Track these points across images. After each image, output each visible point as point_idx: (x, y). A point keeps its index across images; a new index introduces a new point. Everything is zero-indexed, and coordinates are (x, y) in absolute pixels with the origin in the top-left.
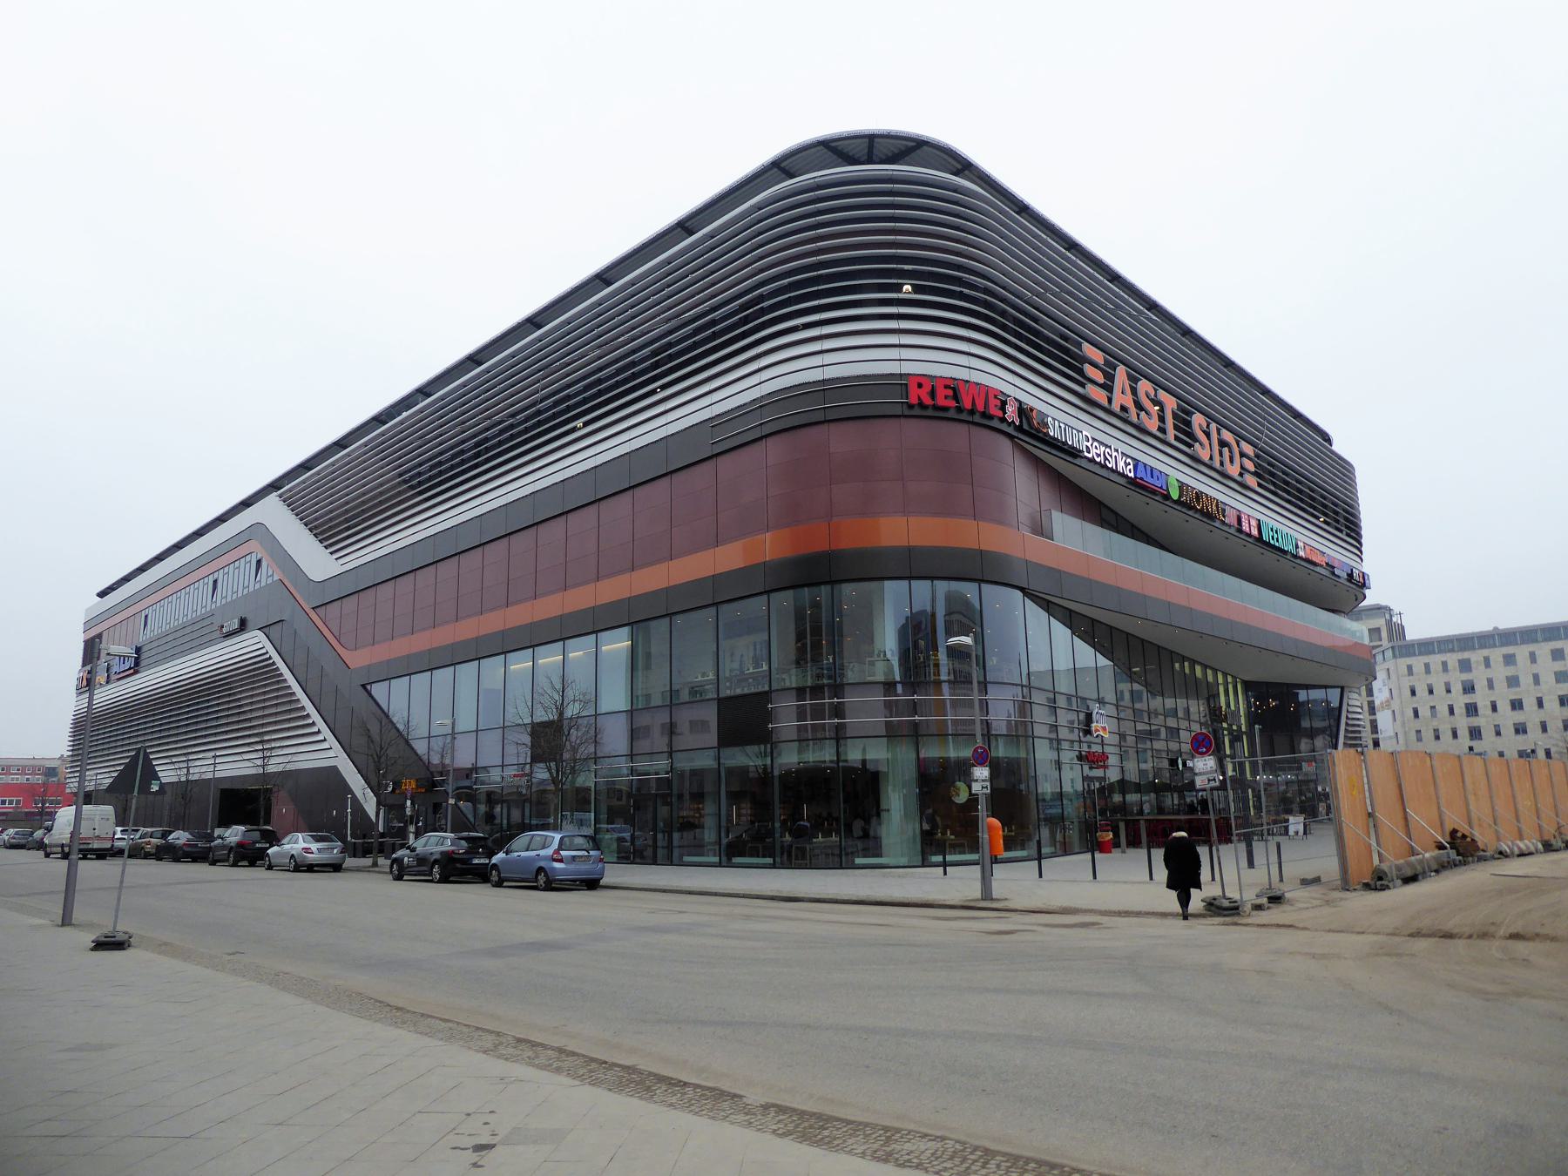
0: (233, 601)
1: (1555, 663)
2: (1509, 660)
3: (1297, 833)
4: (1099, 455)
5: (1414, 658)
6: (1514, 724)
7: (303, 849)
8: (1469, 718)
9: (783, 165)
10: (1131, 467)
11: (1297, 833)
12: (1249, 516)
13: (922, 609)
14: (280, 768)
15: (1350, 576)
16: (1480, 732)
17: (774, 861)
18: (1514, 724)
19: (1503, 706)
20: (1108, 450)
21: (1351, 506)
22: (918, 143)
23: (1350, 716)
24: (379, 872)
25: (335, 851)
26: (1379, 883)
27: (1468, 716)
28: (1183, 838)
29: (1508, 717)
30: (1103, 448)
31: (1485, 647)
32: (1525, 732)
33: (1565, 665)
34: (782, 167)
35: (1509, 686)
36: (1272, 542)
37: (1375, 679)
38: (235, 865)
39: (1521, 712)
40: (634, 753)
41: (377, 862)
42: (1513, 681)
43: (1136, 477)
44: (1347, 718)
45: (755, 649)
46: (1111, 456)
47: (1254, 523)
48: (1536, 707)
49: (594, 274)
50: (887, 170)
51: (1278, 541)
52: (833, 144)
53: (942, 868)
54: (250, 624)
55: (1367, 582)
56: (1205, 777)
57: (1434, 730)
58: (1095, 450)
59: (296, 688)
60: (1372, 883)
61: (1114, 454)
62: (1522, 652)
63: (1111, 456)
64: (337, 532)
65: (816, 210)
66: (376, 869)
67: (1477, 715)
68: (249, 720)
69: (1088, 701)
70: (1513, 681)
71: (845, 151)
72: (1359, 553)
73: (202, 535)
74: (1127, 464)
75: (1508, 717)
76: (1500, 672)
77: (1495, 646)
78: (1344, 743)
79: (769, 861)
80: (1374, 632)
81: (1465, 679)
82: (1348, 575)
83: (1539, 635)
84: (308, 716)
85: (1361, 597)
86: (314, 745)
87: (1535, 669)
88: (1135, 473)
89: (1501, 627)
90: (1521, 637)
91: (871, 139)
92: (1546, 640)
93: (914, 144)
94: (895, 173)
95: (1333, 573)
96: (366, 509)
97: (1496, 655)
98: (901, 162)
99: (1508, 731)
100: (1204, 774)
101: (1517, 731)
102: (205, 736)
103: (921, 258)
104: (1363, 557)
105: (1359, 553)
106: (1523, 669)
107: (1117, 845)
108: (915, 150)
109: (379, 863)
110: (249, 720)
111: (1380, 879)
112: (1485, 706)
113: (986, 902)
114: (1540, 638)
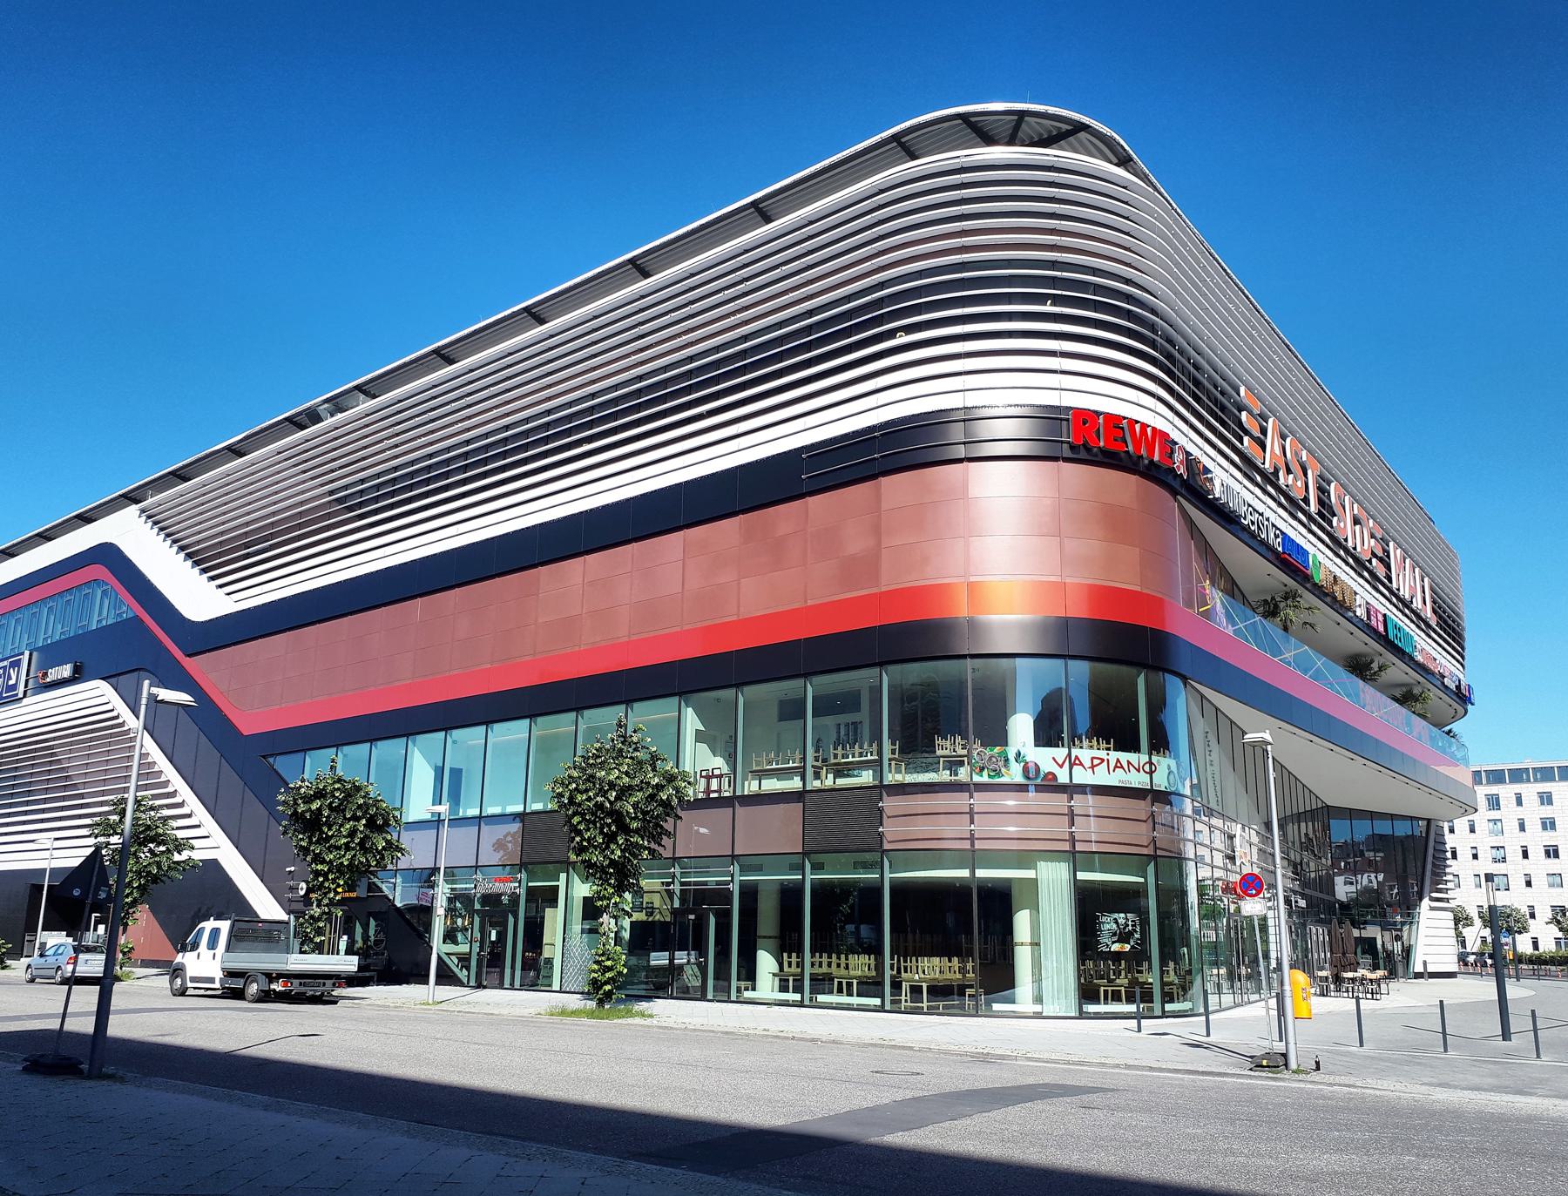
4: (1253, 523)
5: (1553, 784)
10: (1279, 540)
12: (1377, 610)
13: (1053, 688)
15: (1458, 687)
20: (1260, 517)
21: (1458, 625)
30: (1257, 515)
36: (1396, 642)
37: (1476, 810)
40: (479, 864)
43: (1284, 553)
45: (839, 732)
46: (1263, 525)
47: (1380, 618)
51: (1400, 641)
52: (973, 119)
53: (1136, 1021)
55: (1472, 696)
58: (1250, 517)
61: (1266, 523)
63: (1263, 525)
65: (960, 198)
68: (82, 796)
69: (190, 841)
72: (1461, 660)
73: (50, 539)
74: (1276, 536)
76: (1533, 812)
80: (817, 776)
82: (1456, 686)
84: (173, 794)
88: (1283, 548)
90: (1535, 775)
93: (1070, 128)
94: (1061, 159)
96: (276, 521)
97: (1530, 790)
102: (43, 811)
103: (893, 294)
104: (1465, 663)
105: (1461, 660)
110: (82, 796)
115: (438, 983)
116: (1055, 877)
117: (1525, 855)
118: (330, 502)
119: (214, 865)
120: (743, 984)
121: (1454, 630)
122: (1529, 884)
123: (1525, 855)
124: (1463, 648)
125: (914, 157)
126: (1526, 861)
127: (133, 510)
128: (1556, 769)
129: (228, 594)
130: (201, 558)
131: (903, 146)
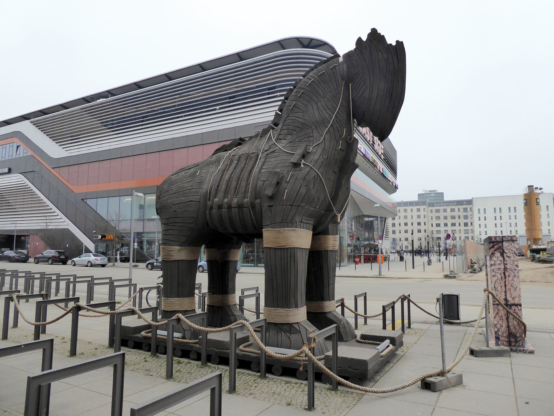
0: (8, 160)
1: (418, 212)
2: (405, 210)
3: (392, 260)
6: (405, 230)
7: (95, 259)
8: (393, 228)
9: (281, 42)
11: (392, 260)
14: (54, 228)
15: (396, 185)
16: (395, 232)
17: (255, 265)
18: (405, 230)
19: (402, 224)
21: (396, 166)
22: (324, 43)
23: (387, 227)
24: (139, 268)
25: (106, 260)
26: (474, 271)
27: (392, 227)
28: (63, 258)
29: (403, 228)
31: (399, 206)
32: (407, 232)
33: (420, 213)
34: (281, 44)
35: (405, 218)
38: (52, 264)
39: (447, 227)
41: (114, 264)
42: (406, 217)
44: (386, 227)
48: (411, 225)
49: (198, 64)
50: (319, 52)
52: (299, 39)
54: (12, 171)
56: (448, 245)
57: (460, 233)
59: (45, 200)
60: (472, 271)
62: (409, 208)
64: (62, 138)
66: (114, 266)
67: (395, 227)
68: (15, 208)
70: (406, 217)
71: (302, 42)
75: (403, 228)
77: (402, 206)
78: (385, 234)
79: (253, 265)
81: (466, 222)
83: (403, 204)
85: (395, 191)
86: (10, 219)
87: (412, 214)
89: (404, 201)
91: (312, 40)
92: (416, 205)
93: (323, 43)
95: (393, 184)
98: (317, 48)
99: (403, 232)
100: (449, 244)
101: (405, 232)
106: (409, 214)
107: (360, 262)
108: (323, 46)
109: (115, 264)
110: (15, 208)
111: (474, 270)
112: (398, 224)
113: (380, 276)
114: (414, 205)
115: (136, 262)
116: (10, 201)
117: (400, 225)
118: (101, 126)
119: (67, 230)
120: (540, 243)
121: (395, 170)
122: (400, 232)
123: (400, 225)
124: (396, 177)
125: (284, 49)
126: (400, 227)
127: (27, 122)
128: (414, 203)
129: (63, 148)
130: (55, 138)
131: (281, 44)
